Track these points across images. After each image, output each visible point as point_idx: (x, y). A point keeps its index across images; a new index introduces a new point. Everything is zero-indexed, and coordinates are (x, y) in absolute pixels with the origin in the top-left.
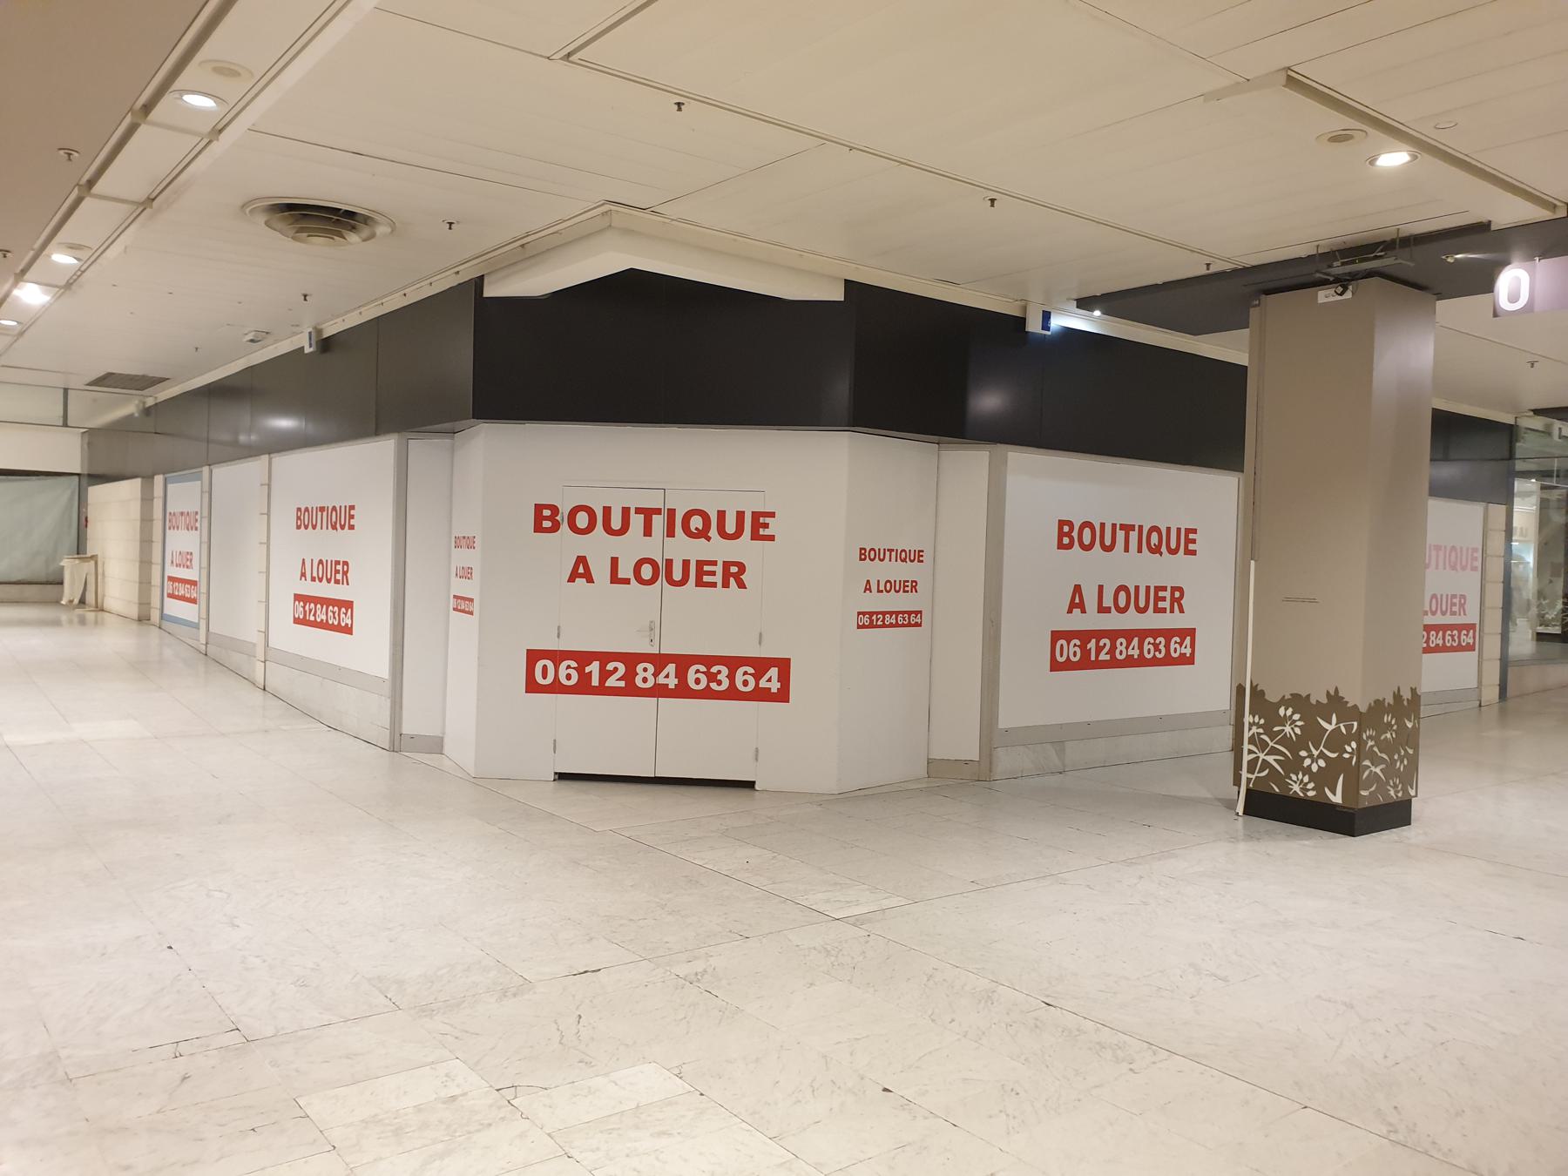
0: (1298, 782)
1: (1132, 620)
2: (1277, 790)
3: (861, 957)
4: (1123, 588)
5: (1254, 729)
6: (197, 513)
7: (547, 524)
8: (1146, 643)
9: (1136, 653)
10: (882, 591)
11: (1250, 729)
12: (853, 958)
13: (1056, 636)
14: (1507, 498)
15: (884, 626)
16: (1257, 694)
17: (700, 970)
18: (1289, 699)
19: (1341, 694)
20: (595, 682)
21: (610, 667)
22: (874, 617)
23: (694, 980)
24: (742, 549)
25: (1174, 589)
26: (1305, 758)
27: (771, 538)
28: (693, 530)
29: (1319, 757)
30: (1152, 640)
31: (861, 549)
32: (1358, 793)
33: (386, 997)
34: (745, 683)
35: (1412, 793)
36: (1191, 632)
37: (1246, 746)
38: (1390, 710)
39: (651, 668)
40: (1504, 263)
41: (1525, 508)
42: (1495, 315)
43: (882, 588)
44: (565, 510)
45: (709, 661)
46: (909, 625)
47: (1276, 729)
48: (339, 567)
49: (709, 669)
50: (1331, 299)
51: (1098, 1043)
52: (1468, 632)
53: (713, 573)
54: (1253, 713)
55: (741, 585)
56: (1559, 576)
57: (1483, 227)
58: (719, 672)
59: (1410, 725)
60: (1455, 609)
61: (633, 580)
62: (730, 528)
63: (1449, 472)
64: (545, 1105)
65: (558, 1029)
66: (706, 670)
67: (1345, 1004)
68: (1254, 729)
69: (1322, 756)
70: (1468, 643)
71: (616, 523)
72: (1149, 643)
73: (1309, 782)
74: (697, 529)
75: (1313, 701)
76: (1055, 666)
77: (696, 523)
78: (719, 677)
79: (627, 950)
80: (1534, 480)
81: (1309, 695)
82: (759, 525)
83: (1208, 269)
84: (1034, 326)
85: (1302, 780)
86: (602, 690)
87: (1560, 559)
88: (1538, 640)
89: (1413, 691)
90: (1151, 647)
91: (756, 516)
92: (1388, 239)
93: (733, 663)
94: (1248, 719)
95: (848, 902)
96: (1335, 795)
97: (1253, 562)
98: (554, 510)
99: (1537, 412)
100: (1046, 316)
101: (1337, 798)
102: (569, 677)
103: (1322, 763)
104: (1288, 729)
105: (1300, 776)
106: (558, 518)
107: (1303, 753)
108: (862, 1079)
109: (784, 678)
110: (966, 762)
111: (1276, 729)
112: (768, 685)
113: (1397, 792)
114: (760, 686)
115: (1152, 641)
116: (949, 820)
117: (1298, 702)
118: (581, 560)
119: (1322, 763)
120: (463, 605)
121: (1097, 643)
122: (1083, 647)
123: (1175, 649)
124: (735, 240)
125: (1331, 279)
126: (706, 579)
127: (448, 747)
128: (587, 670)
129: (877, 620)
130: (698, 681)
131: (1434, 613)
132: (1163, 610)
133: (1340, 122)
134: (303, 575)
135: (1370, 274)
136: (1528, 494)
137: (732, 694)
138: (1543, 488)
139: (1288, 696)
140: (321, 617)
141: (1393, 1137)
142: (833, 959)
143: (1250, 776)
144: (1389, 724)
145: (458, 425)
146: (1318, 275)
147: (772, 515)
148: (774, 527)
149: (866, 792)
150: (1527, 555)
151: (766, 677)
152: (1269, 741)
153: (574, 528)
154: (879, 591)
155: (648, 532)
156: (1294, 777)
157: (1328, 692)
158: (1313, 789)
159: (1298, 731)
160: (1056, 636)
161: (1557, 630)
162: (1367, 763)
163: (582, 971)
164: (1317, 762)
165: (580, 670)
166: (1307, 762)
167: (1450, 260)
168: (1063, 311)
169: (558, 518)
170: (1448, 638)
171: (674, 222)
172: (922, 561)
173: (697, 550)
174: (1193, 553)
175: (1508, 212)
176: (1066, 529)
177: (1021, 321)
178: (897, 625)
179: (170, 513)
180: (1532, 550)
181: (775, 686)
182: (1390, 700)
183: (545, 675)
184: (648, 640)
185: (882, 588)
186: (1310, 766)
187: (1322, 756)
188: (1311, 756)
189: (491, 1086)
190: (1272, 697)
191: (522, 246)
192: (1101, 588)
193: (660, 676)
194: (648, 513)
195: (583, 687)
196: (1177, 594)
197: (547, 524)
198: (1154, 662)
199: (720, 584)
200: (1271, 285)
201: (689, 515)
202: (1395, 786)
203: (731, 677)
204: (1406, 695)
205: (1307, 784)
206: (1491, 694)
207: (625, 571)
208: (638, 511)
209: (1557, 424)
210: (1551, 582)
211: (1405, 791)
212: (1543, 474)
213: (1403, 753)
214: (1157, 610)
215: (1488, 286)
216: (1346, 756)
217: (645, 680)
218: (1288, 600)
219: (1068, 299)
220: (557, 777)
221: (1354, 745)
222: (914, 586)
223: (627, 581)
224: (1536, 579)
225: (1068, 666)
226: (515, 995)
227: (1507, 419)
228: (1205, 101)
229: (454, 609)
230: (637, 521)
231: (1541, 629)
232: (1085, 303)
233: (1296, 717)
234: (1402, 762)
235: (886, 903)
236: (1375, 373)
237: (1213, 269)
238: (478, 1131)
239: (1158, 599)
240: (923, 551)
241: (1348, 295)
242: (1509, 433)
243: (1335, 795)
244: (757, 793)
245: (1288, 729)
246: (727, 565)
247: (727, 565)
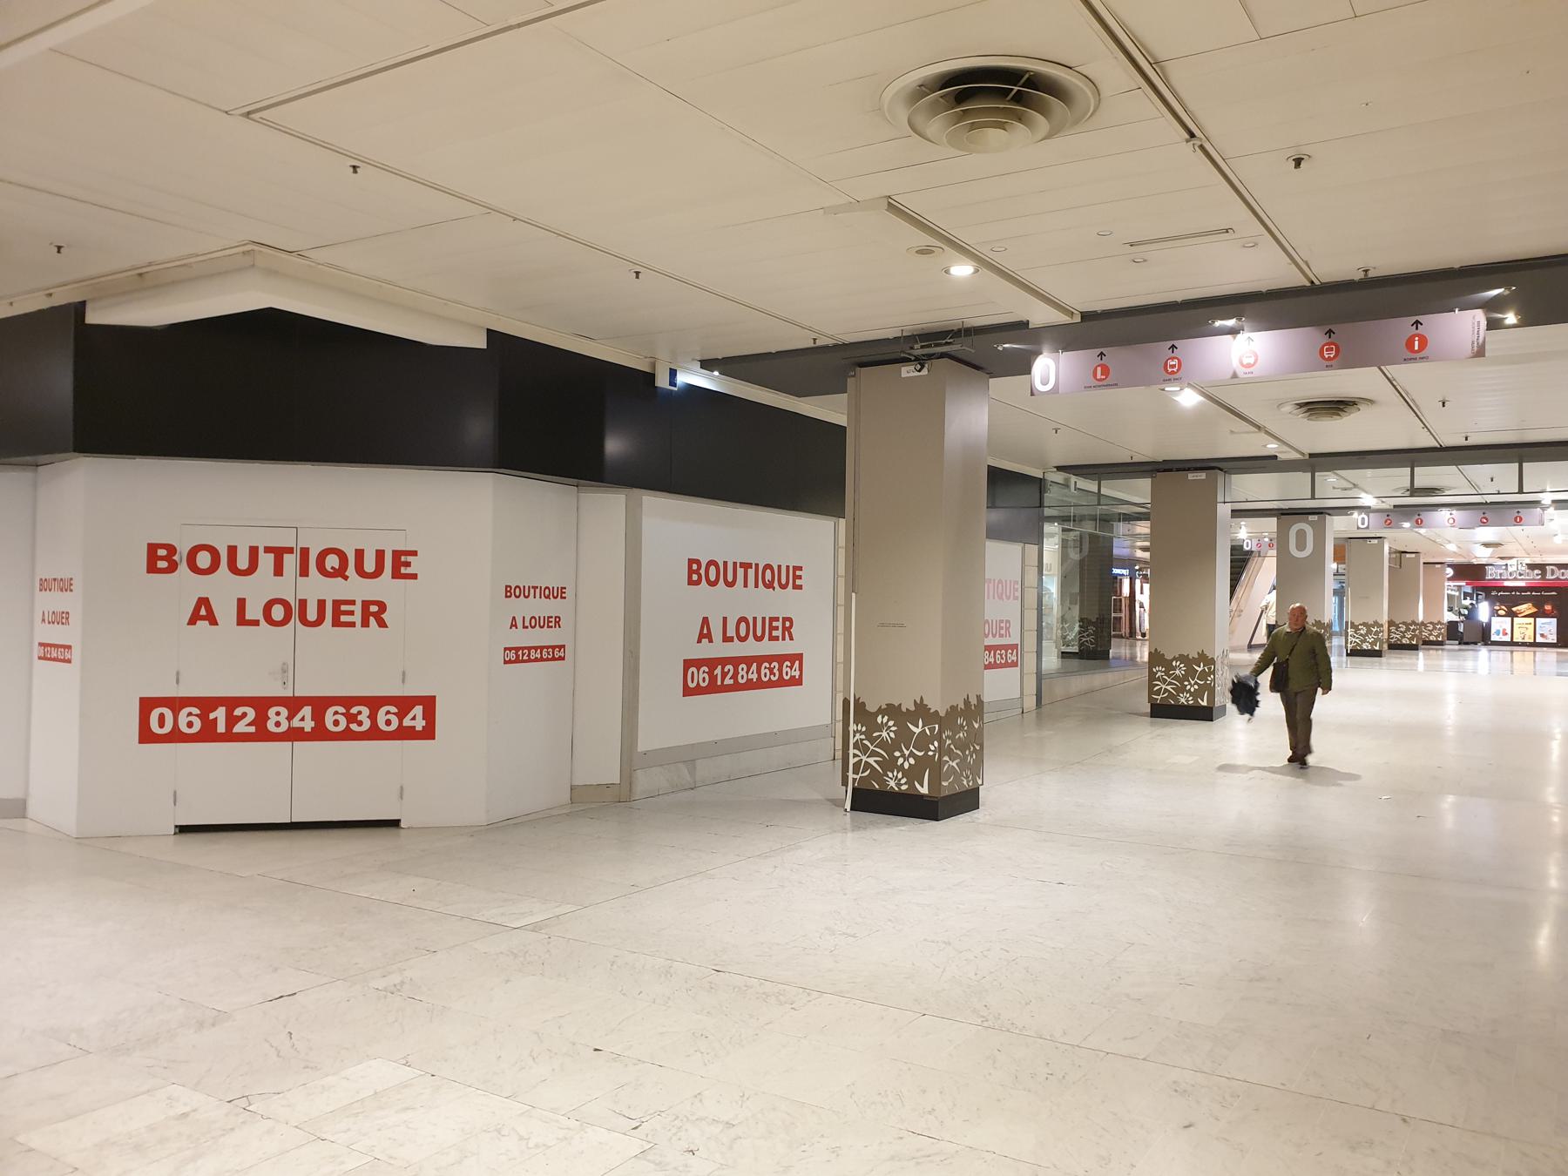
1: (751, 648)
2: (877, 787)
3: (547, 956)
4: (743, 619)
5: (858, 736)
7: (162, 564)
8: (763, 668)
9: (754, 677)
10: (527, 627)
11: (854, 736)
12: (540, 957)
13: (688, 664)
14: (1039, 539)
15: (529, 660)
16: (860, 706)
17: (397, 982)
18: (885, 709)
19: (925, 703)
20: (221, 728)
21: (238, 712)
22: (520, 653)
23: (394, 990)
24: (383, 588)
25: (785, 619)
27: (414, 576)
28: (329, 569)
29: (909, 756)
30: (767, 665)
31: (507, 587)
32: (940, 783)
33: (69, 1045)
34: (388, 723)
35: (980, 782)
36: (799, 657)
37: (852, 751)
39: (284, 712)
40: (1038, 353)
41: (1051, 547)
42: (1032, 394)
43: (527, 624)
44: (183, 549)
45: (348, 702)
46: (554, 659)
47: (874, 735)
48: (64, 615)
49: (348, 709)
50: (912, 374)
51: (764, 993)
52: (1013, 651)
53: (351, 613)
54: (856, 722)
55: (382, 624)
56: (1076, 604)
57: (1024, 325)
58: (360, 713)
59: (976, 726)
60: (1003, 632)
61: (262, 622)
62: (370, 566)
63: (997, 516)
64: (283, 1106)
65: (272, 1047)
66: (344, 711)
67: (945, 942)
68: (858, 736)
69: (1196, 683)
70: (1013, 661)
71: (243, 562)
72: (766, 668)
73: (903, 778)
74: (332, 568)
75: (904, 710)
76: (688, 692)
77: (332, 562)
78: (359, 718)
79: (317, 974)
80: (1056, 524)
81: (900, 704)
82: (401, 564)
83: (815, 343)
84: (662, 382)
86: (230, 737)
87: (1076, 589)
88: (1062, 657)
89: (978, 697)
90: (767, 671)
91: (397, 555)
92: (955, 328)
93: (374, 703)
94: (852, 727)
95: (522, 914)
97: (854, 594)
98: (171, 550)
99: (1060, 468)
100: (673, 373)
101: (924, 790)
102: (190, 725)
103: (1196, 687)
104: (884, 734)
105: (895, 773)
106: (176, 558)
107: (897, 754)
108: (574, 1044)
109: (430, 715)
110: (608, 786)
111: (874, 735)
112: (412, 723)
113: (968, 782)
114: (404, 725)
115: (768, 666)
116: (599, 837)
117: (892, 711)
118: (203, 602)
119: (912, 761)
120: (55, 653)
121: (723, 669)
122: (711, 673)
123: (787, 672)
124: (380, 286)
125: (913, 358)
126: (344, 618)
127: (32, 810)
128: (212, 716)
129: (523, 655)
130: (336, 723)
131: (994, 636)
132: (776, 639)
133: (926, 240)
134: (43, 620)
135: (942, 355)
136: (1052, 535)
137: (374, 734)
138: (1064, 530)
139: (884, 707)
140: (54, 655)
141: (986, 1024)
142: (521, 959)
143: (855, 776)
144: (962, 725)
145: (42, 458)
146: (902, 355)
147: (414, 553)
148: (416, 565)
149: (530, 817)
150: (1052, 586)
151: (411, 715)
152: (869, 745)
153: (194, 568)
154: (525, 627)
155: (278, 571)
158: (905, 784)
159: (892, 735)
160: (688, 664)
161: (1075, 649)
162: (946, 758)
163: (277, 996)
165: (203, 717)
166: (901, 761)
167: (1000, 348)
168: (687, 370)
169: (176, 558)
170: (998, 656)
171: (320, 266)
172: (565, 598)
173: (333, 589)
174: (800, 587)
175: (1041, 315)
176: (695, 567)
177: (650, 377)
178: (542, 659)
179: (41, 579)
180: (1056, 579)
181: (420, 724)
182: (962, 706)
183: (162, 724)
184: (281, 683)
185: (527, 624)
187: (1196, 683)
188: (903, 755)
189: (221, 1100)
190: (872, 708)
191: (140, 275)
192: (725, 619)
193: (294, 720)
194: (279, 553)
195: (209, 734)
196: (788, 624)
197: (162, 564)
198: (770, 685)
199: (359, 623)
200: (865, 359)
201: (323, 555)
202: (967, 777)
203: (373, 717)
204: (973, 701)
206: (1030, 702)
207: (255, 611)
208: (268, 550)
209: (1073, 479)
210: (1070, 609)
211: (974, 780)
212: (1063, 519)
213: (972, 748)
214: (772, 638)
215: (1026, 369)
216: (930, 753)
217: (278, 724)
218: (883, 625)
219: (693, 360)
220: (177, 831)
221: (936, 744)
222: (558, 621)
223: (256, 623)
224: (1060, 607)
225: (699, 691)
226: (213, 1025)
227: (1038, 474)
228: (825, 213)
229: (40, 658)
230: (266, 561)
231: (1064, 649)
232: (707, 364)
233: (891, 723)
234: (972, 756)
235: (559, 911)
236: (946, 436)
237: (819, 343)
238: (223, 1135)
239: (772, 628)
240: (565, 588)
241: (925, 372)
242: (1040, 484)
244: (402, 830)
245: (884, 734)
246: (366, 604)
247: (366, 604)
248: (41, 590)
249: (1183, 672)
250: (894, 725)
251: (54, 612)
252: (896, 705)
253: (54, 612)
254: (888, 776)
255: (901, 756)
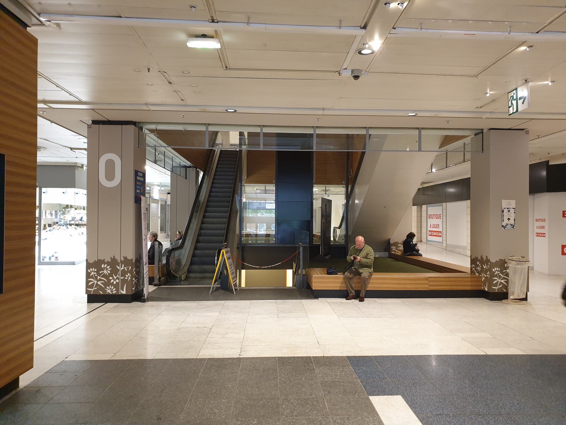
0: (110, 289)
2: (102, 293)
6: (440, 214)
18: (499, 261)
19: (115, 258)
26: (111, 279)
29: (116, 279)
38: (479, 261)
47: (101, 272)
48: (437, 225)
60: (437, 227)
69: (118, 278)
73: (114, 288)
81: (505, 259)
85: (111, 288)
96: (123, 291)
103: (117, 281)
104: (105, 272)
105: (110, 287)
107: (111, 278)
111: (101, 272)
134: (431, 227)
154: (433, 228)
156: (108, 288)
157: (111, 257)
158: (115, 291)
159: (109, 272)
164: (116, 281)
166: (112, 281)
179: (429, 215)
182: (479, 258)
186: (113, 282)
188: (114, 279)
205: (113, 289)
233: (108, 267)
243: (123, 291)
245: (105, 272)
248: (429, 218)
249: (402, 248)
250: (109, 268)
251: (434, 224)
252: (102, 260)
253: (434, 224)
254: (107, 289)
255: (113, 279)
